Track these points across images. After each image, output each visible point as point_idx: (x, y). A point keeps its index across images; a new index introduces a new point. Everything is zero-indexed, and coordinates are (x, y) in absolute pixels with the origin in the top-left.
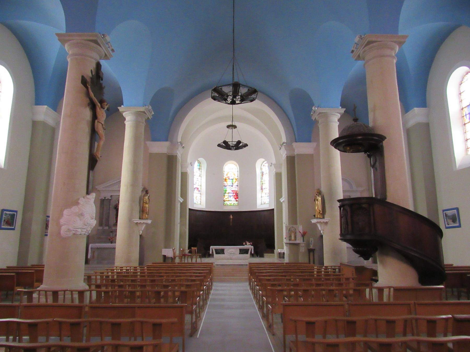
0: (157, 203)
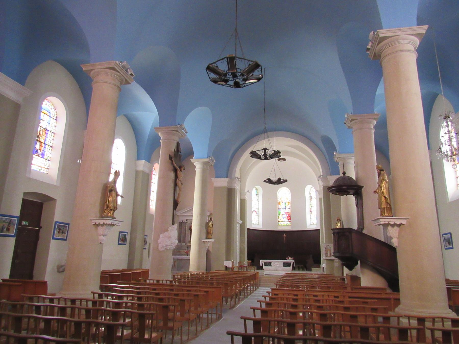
0: (219, 228)
